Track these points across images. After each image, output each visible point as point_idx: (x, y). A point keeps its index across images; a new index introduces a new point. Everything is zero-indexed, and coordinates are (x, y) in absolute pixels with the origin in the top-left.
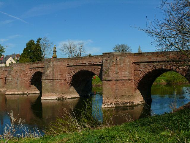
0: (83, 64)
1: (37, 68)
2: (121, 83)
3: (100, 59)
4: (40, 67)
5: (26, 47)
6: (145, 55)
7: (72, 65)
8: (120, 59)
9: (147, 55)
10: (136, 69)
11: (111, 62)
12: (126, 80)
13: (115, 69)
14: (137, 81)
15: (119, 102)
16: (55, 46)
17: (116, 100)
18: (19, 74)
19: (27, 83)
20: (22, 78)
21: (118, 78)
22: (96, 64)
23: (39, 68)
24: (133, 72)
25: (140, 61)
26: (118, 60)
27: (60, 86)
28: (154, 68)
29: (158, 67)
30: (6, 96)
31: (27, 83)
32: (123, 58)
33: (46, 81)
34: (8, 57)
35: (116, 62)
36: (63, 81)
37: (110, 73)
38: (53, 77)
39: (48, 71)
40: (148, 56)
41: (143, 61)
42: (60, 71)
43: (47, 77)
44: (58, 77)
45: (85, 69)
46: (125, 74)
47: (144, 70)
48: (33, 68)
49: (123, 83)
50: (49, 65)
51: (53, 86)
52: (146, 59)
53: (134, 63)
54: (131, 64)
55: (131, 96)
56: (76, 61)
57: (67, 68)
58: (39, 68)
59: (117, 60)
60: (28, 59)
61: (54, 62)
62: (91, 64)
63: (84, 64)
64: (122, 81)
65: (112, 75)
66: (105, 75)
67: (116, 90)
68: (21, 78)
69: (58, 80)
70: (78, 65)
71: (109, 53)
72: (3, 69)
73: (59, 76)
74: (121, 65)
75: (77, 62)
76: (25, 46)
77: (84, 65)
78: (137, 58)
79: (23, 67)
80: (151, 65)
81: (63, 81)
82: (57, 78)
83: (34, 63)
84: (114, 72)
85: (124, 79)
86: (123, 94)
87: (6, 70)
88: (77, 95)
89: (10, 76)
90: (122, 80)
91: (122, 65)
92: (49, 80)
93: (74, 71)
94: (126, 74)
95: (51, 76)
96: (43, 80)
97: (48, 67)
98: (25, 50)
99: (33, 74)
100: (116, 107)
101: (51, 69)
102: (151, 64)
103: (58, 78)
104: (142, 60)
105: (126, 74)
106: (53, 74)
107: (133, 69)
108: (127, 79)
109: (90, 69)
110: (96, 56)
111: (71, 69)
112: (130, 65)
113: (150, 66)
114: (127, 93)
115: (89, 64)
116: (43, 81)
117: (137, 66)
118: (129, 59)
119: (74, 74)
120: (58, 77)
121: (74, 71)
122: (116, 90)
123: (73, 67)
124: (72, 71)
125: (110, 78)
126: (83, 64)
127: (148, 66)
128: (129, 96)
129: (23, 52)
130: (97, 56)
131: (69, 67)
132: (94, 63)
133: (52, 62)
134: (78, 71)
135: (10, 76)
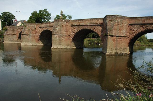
0: (85, 24)
1: (45, 27)
2: (119, 39)
3: (100, 21)
4: (48, 26)
5: (32, 16)
6: (140, 19)
7: (75, 25)
9: (141, 19)
10: (131, 29)
11: (114, 22)
12: (123, 36)
13: (117, 28)
14: (131, 38)
16: (62, 10)
17: (116, 51)
18: (31, 31)
19: (37, 38)
20: (34, 34)
21: (118, 35)
22: (97, 24)
23: (47, 27)
24: (128, 31)
25: (134, 23)
26: (119, 21)
27: (65, 40)
28: (146, 29)
29: (150, 28)
30: (21, 45)
31: (37, 38)
32: (122, 20)
33: (55, 36)
34: (19, 22)
35: (118, 22)
36: (68, 37)
37: (114, 31)
38: (60, 33)
39: (57, 29)
40: (142, 20)
41: (138, 23)
42: (66, 29)
43: (56, 33)
44: (64, 33)
45: (86, 28)
47: (136, 30)
48: (42, 27)
49: (121, 39)
50: (58, 24)
51: (60, 40)
52: (140, 22)
53: (130, 25)
54: (127, 25)
55: (125, 49)
56: (79, 22)
57: (71, 27)
58: (47, 27)
61: (62, 22)
62: (92, 24)
63: (86, 24)
64: (120, 38)
65: (115, 32)
66: (109, 31)
68: (32, 34)
69: (64, 36)
70: (80, 25)
71: (113, 15)
72: (17, 28)
73: (65, 33)
75: (80, 23)
76: (31, 15)
77: (86, 25)
78: (132, 21)
79: (34, 26)
80: (144, 27)
81: (68, 37)
82: (63, 34)
83: (43, 24)
84: (116, 30)
85: (122, 36)
87: (20, 29)
88: (75, 47)
89: (24, 32)
91: (122, 25)
93: (77, 30)
94: (123, 32)
95: (59, 33)
96: (53, 35)
97: (57, 26)
98: (31, 18)
99: (41, 31)
101: (60, 27)
102: (144, 26)
103: (65, 34)
104: (136, 22)
105: (123, 32)
106: (61, 31)
107: (128, 29)
108: (124, 36)
109: (91, 28)
110: (97, 18)
111: (74, 28)
112: (126, 25)
113: (143, 27)
115: (90, 24)
116: (53, 36)
117: (132, 27)
118: (126, 21)
119: (77, 31)
120: (64, 33)
121: (77, 30)
123: (77, 26)
124: (75, 29)
125: (113, 35)
126: (85, 24)
127: (142, 27)
129: (29, 19)
130: (98, 18)
131: (73, 27)
132: (94, 24)
133: (60, 22)
134: (80, 29)
135: (24, 32)
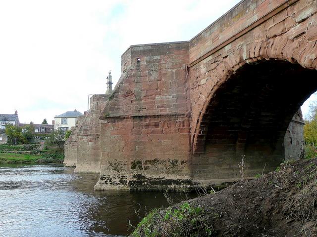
8: (149, 62)
12: (167, 115)
15: (144, 177)
21: (143, 113)
32: (156, 58)
43: (86, 130)
46: (162, 101)
59: (142, 63)
60: (129, 67)
67: (136, 143)
74: (151, 75)
86: (159, 156)
90: (155, 116)
92: (90, 137)
100: (132, 191)
110: (196, 37)
114: (168, 153)
122: (136, 143)
125: (121, 113)
128: (177, 161)
